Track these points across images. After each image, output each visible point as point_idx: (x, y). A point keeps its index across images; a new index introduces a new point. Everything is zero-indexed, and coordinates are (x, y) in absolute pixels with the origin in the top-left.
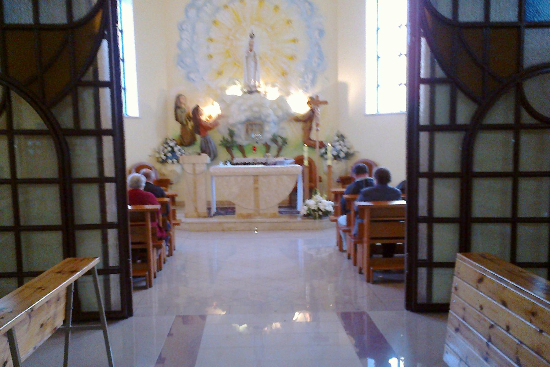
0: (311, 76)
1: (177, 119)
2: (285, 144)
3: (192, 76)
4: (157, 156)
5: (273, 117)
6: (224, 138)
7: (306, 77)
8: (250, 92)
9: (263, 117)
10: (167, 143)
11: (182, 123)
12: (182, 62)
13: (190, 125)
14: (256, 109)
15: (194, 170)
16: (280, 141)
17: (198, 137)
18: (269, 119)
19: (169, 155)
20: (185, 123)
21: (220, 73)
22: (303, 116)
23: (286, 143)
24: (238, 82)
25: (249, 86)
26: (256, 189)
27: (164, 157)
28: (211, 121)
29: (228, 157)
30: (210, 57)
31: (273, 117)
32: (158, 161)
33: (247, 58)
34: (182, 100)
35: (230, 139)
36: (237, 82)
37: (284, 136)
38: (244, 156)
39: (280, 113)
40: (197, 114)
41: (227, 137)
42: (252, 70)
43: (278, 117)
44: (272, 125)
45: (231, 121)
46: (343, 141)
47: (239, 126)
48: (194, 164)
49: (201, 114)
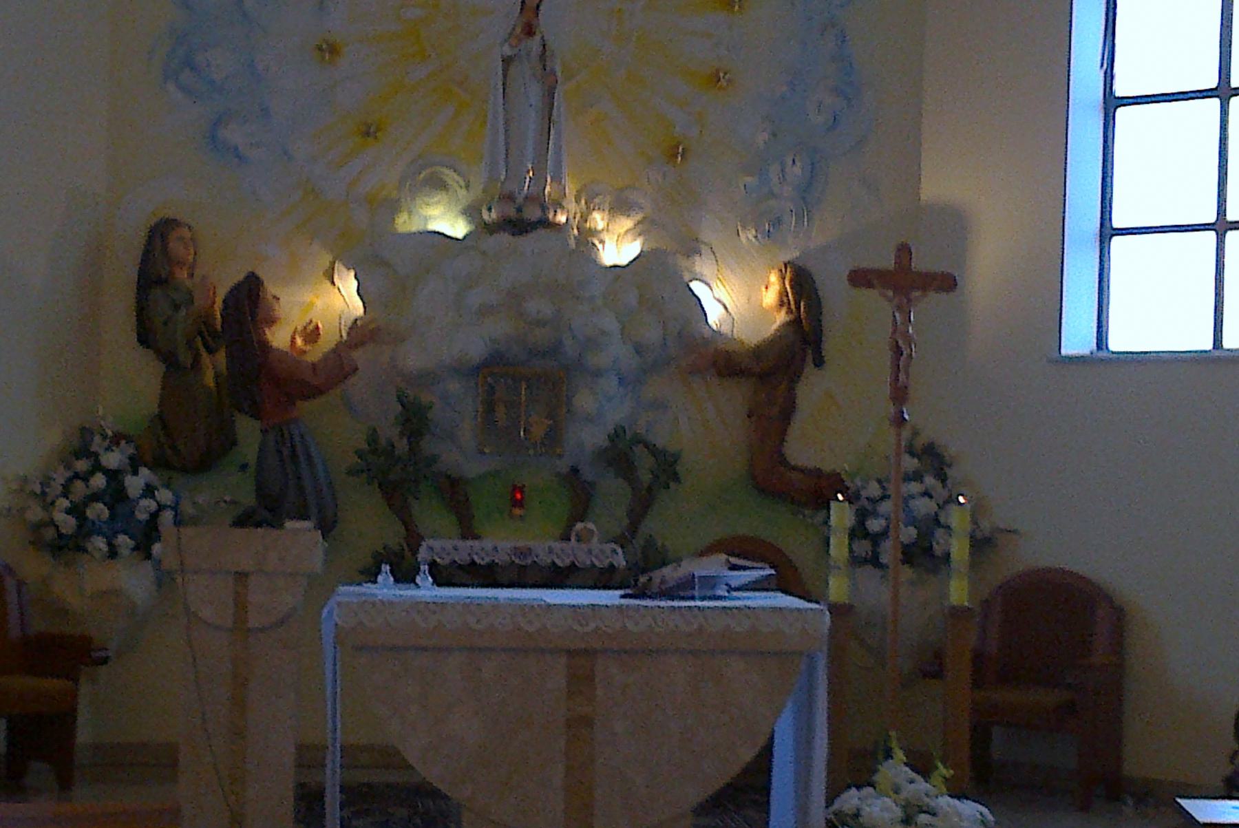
0: (796, 171)
1: (145, 338)
2: (672, 484)
3: (233, 134)
4: (36, 513)
5: (616, 352)
6: (373, 437)
7: (774, 170)
8: (517, 226)
9: (570, 348)
10: (84, 451)
11: (169, 359)
12: (189, 64)
13: (213, 366)
14: (539, 306)
15: (241, 605)
16: (645, 466)
17: (248, 431)
18: (598, 360)
19: (98, 511)
20: (185, 358)
21: (369, 132)
22: (758, 352)
23: (676, 478)
24: (456, 176)
25: (509, 198)
26: (579, 725)
27: (68, 524)
28: (315, 354)
29: (393, 535)
30: (329, 50)
31: (616, 352)
32: (37, 543)
33: (507, 61)
34: (175, 247)
35: (402, 446)
36: (450, 176)
37: (661, 439)
38: (468, 532)
39: (651, 333)
40: (253, 315)
41: (390, 431)
42: (531, 122)
43: (639, 349)
44: (609, 384)
45: (413, 359)
46: (942, 478)
47: (454, 386)
48: (241, 576)
49: (272, 321)
